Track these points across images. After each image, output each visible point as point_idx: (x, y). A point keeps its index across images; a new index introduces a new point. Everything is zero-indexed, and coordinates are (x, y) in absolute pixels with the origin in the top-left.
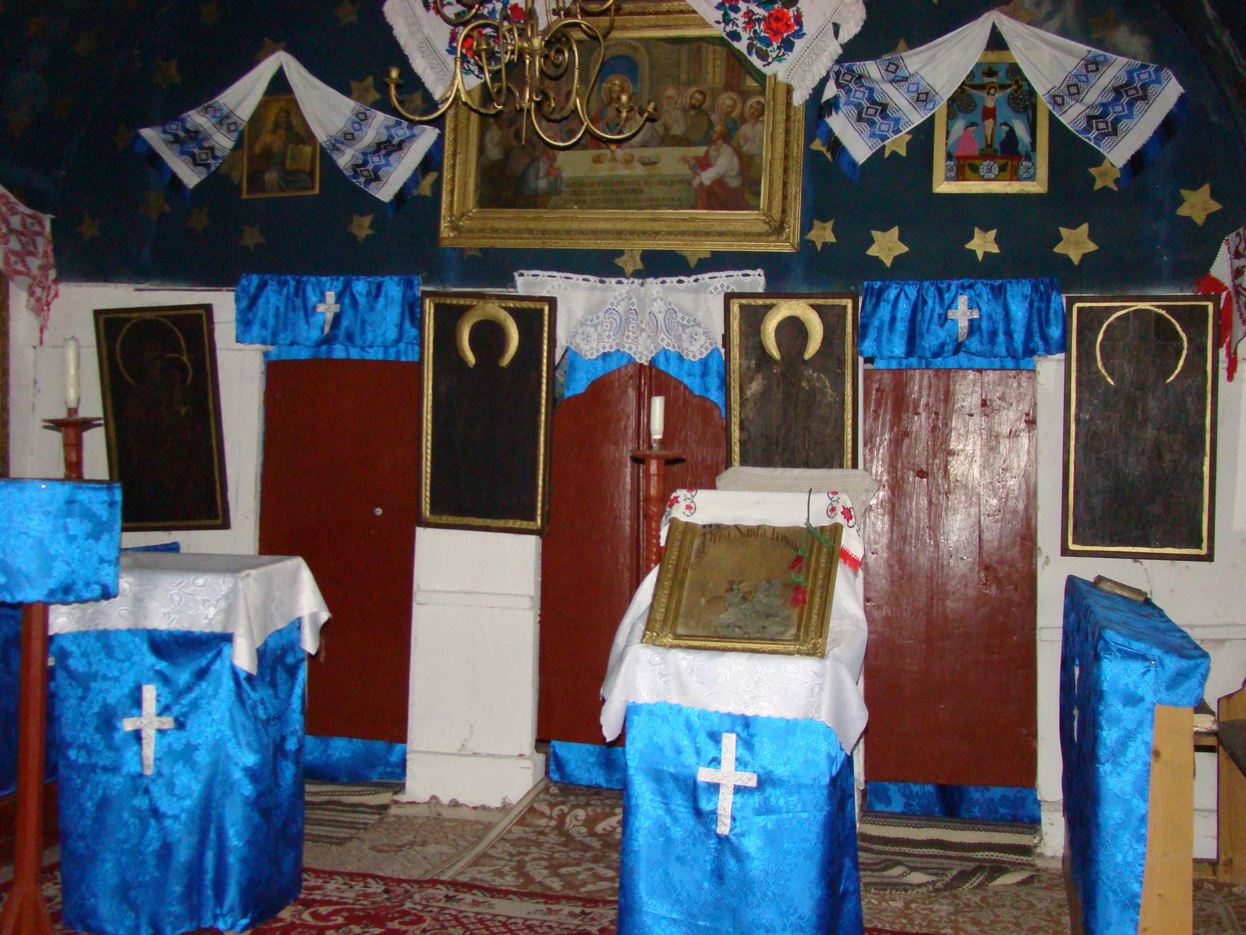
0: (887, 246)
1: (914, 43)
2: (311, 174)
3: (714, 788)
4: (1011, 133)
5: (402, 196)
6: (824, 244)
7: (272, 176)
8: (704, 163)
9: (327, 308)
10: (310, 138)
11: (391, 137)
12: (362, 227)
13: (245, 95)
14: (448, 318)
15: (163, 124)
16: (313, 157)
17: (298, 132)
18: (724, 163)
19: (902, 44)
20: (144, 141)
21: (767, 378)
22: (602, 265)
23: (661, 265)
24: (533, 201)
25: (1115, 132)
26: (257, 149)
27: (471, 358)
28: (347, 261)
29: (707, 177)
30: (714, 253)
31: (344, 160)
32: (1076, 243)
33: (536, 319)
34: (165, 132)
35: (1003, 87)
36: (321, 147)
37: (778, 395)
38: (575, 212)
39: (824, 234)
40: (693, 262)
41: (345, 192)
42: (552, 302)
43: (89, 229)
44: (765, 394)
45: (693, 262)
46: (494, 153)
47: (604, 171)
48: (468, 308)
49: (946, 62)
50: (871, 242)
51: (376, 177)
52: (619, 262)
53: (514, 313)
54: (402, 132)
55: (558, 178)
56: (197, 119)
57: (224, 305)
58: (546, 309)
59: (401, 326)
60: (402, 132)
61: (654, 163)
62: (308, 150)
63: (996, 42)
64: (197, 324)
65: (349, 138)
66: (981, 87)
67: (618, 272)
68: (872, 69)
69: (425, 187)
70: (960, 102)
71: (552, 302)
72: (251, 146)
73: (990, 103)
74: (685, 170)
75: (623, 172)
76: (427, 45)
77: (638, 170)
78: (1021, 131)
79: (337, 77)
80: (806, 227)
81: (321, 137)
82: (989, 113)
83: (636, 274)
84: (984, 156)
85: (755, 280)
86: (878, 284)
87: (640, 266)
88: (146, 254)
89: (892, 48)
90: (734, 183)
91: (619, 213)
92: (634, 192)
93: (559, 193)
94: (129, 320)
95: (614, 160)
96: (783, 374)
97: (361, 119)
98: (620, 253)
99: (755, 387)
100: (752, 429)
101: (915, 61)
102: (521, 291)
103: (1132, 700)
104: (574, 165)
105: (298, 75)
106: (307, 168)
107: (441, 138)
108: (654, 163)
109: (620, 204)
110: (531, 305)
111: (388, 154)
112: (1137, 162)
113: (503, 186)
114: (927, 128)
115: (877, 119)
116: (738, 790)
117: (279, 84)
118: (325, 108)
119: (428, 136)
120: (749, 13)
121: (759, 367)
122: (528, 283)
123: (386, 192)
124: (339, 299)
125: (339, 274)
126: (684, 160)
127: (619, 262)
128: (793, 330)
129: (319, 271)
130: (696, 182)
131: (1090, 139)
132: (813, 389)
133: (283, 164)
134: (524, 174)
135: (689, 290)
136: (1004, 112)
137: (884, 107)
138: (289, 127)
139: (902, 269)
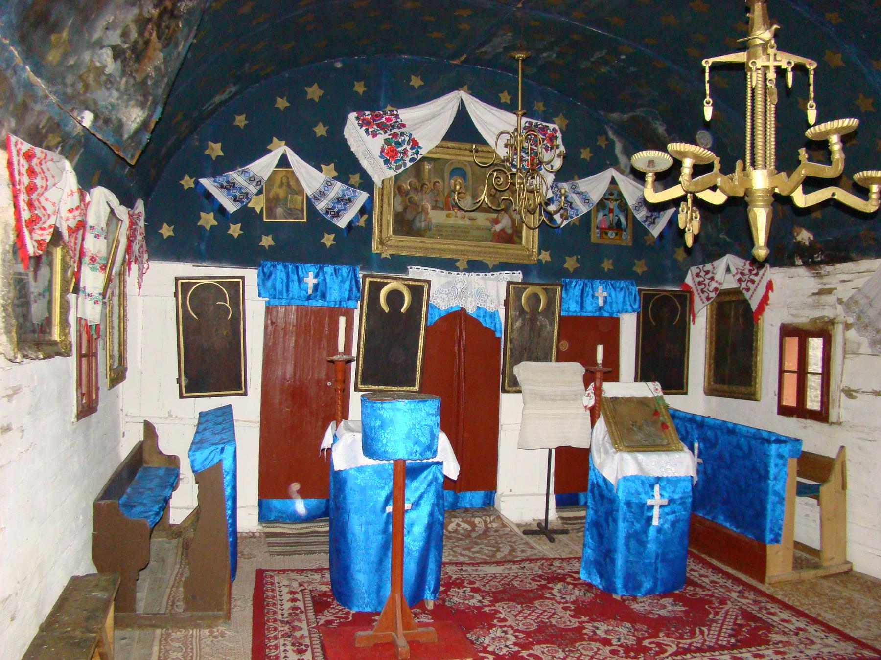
0: (570, 263)
1: (580, 178)
2: (302, 210)
3: (652, 507)
4: (619, 220)
5: (350, 226)
6: (170, 226)
7: (279, 210)
8: (496, 222)
9: (310, 280)
10: (300, 191)
11: (344, 195)
12: (328, 240)
13: (263, 166)
14: (376, 288)
15: (214, 177)
16: (303, 203)
17: (293, 186)
18: (505, 222)
19: (576, 177)
20: (202, 186)
21: (523, 320)
22: (448, 265)
23: (476, 267)
24: (419, 233)
25: (654, 223)
26: (271, 195)
27: (386, 309)
28: (321, 258)
29: (498, 228)
30: (500, 263)
31: (321, 206)
32: (640, 267)
33: (418, 290)
34: (215, 182)
35: (616, 200)
36: (307, 196)
37: (527, 328)
38: (438, 240)
39: (545, 256)
40: (491, 267)
41: (318, 222)
42: (429, 282)
43: (167, 231)
44: (522, 327)
45: (491, 267)
46: (400, 209)
47: (451, 221)
48: (387, 283)
49: (595, 186)
50: (565, 262)
51: (337, 215)
52: (457, 264)
53: (409, 286)
54: (349, 193)
55: (430, 222)
56: (235, 176)
57: (251, 276)
58: (370, 279)
59: (351, 290)
60: (349, 193)
61: (474, 220)
62: (299, 198)
63: (613, 182)
64: (235, 287)
65: (322, 194)
66: (608, 199)
67: (456, 269)
68: (565, 186)
69: (362, 222)
70: (601, 205)
71: (429, 282)
72: (268, 192)
73: (612, 207)
74: (488, 224)
75: (461, 222)
76: (368, 153)
77: (467, 222)
78: (623, 220)
79: (315, 160)
80: (539, 253)
81: (309, 191)
82: (611, 211)
83: (465, 270)
84: (610, 228)
85: (518, 276)
86: (568, 280)
87: (467, 267)
88: (203, 247)
89: (572, 179)
90: (510, 231)
91: (443, 241)
92: (465, 232)
93: (430, 230)
94: (195, 283)
95: (456, 216)
96: (530, 319)
97: (328, 184)
98: (458, 260)
99: (518, 324)
100: (516, 343)
101: (584, 185)
102: (410, 276)
103: (781, 456)
104: (437, 217)
105: (294, 158)
106: (299, 207)
107: (371, 199)
108: (474, 220)
109: (459, 238)
110: (420, 284)
111: (345, 204)
112: (661, 235)
113: (405, 224)
114: (588, 215)
115: (569, 208)
116: (661, 506)
117: (284, 162)
118: (311, 178)
119: (362, 197)
120: (522, 157)
121: (520, 315)
122: (416, 272)
123: (342, 223)
124: (316, 276)
125: (317, 263)
126: (487, 219)
127: (457, 264)
128: (535, 298)
129: (306, 261)
130: (493, 230)
131: (646, 225)
132: (542, 325)
133: (286, 205)
134: (414, 220)
135: (437, 275)
136: (616, 211)
137: (571, 203)
138: (289, 186)
139: (576, 274)
